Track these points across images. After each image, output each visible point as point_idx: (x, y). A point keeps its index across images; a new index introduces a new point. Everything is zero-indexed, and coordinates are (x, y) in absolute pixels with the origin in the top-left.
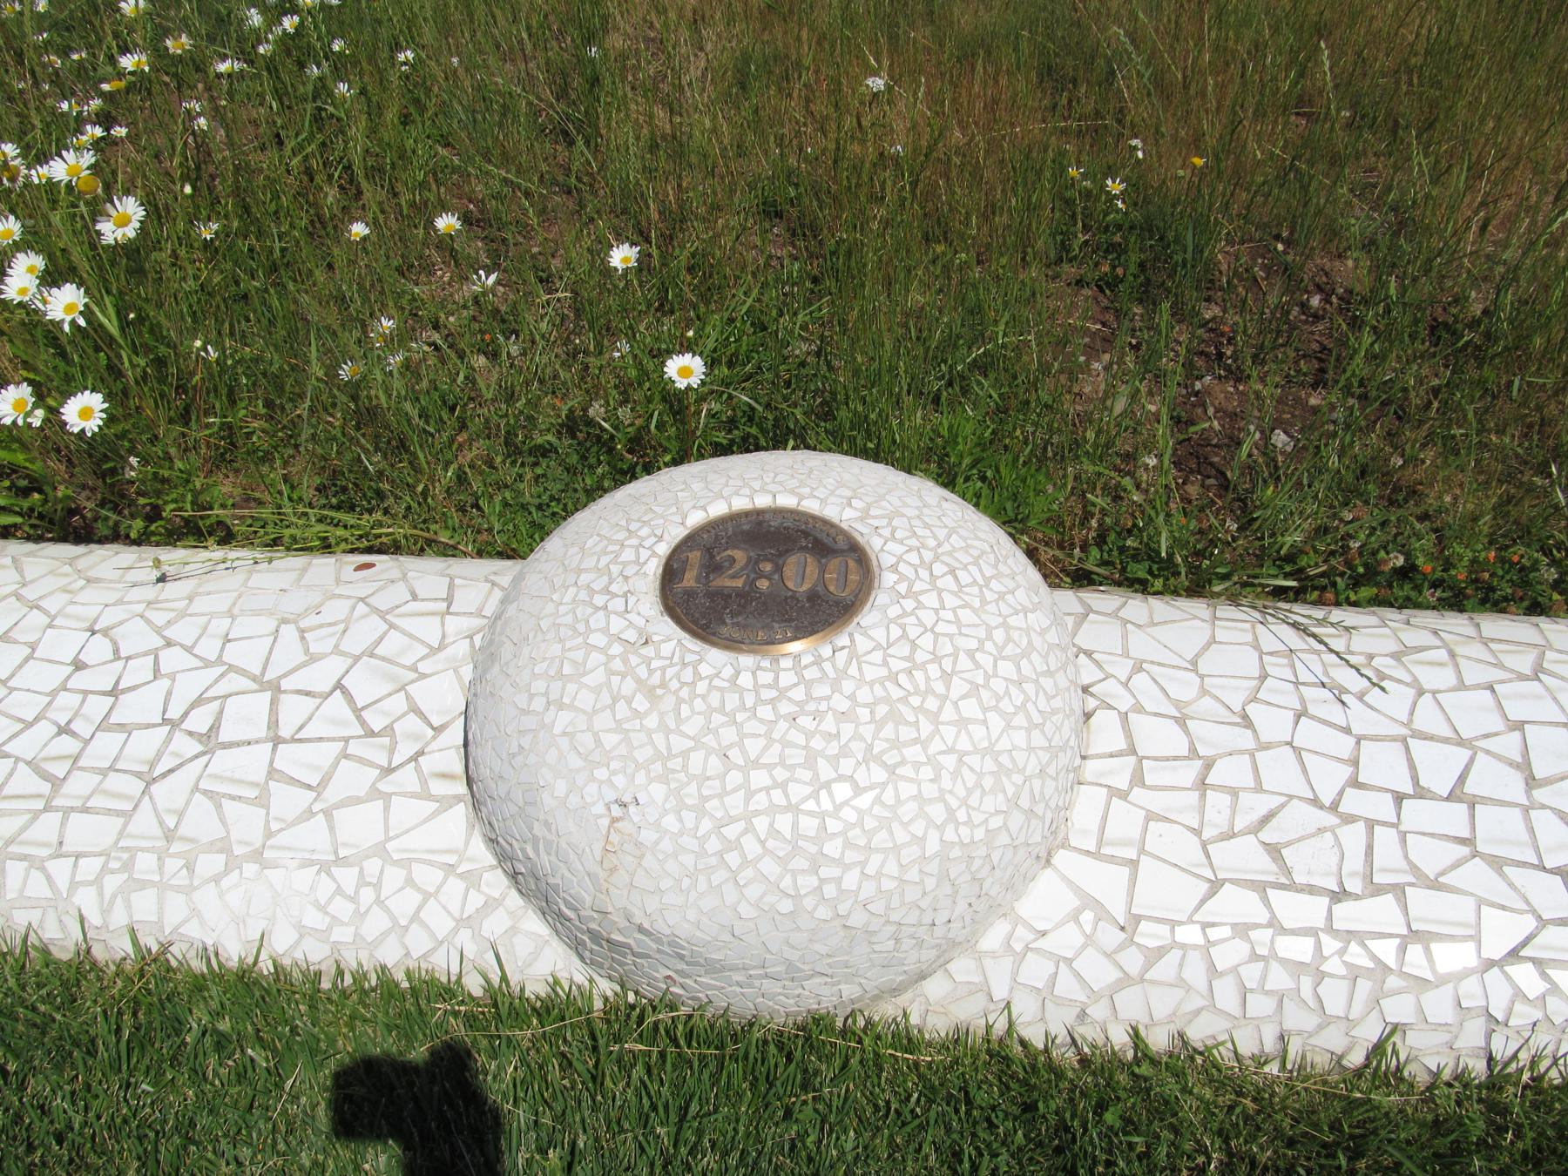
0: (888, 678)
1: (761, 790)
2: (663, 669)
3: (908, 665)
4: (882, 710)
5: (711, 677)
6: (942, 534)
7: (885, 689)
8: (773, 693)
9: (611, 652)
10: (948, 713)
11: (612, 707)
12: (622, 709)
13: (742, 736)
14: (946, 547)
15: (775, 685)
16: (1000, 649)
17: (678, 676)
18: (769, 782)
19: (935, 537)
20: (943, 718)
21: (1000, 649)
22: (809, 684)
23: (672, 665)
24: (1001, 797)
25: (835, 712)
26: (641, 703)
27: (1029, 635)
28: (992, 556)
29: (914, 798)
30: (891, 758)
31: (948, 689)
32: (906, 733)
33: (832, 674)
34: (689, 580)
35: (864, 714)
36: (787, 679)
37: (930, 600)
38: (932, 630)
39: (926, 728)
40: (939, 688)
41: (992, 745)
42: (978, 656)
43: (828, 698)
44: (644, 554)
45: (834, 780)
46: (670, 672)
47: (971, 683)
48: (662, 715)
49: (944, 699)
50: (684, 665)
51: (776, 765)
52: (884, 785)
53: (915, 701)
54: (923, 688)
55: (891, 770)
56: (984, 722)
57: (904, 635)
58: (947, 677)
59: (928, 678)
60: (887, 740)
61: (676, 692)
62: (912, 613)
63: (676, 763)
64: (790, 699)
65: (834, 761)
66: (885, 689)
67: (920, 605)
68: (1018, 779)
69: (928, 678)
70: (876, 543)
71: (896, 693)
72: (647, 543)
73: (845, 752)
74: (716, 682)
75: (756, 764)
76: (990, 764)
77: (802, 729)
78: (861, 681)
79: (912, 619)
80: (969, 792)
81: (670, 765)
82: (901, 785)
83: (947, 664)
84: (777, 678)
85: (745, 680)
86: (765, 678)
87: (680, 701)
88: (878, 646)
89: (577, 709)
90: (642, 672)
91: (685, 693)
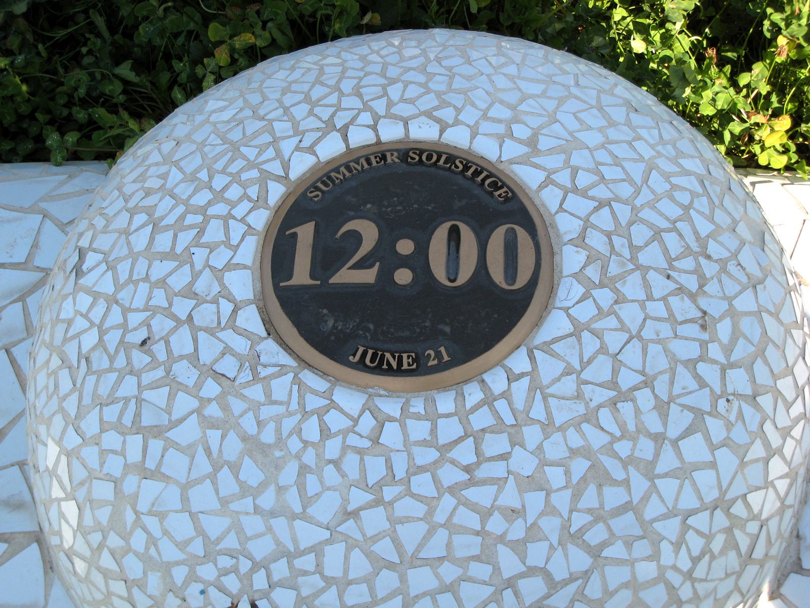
0: (586, 418)
1: (424, 594)
2: (278, 420)
3: (613, 393)
4: (580, 466)
5: (345, 433)
6: (637, 171)
7: (583, 436)
8: (432, 455)
9: (204, 393)
10: (667, 461)
11: (213, 477)
12: (227, 482)
13: (394, 521)
14: (645, 196)
15: (431, 442)
16: (728, 350)
17: (297, 431)
18: (434, 584)
19: (629, 180)
20: (660, 468)
21: (728, 350)
22: (478, 437)
23: (290, 414)
24: (732, 555)
25: (517, 476)
26: (252, 473)
27: (761, 321)
28: (704, 200)
29: (626, 585)
30: (596, 535)
31: (665, 424)
32: (614, 497)
33: (509, 420)
34: (301, 275)
35: (555, 475)
36: (449, 430)
37: (632, 288)
38: (639, 336)
39: (639, 484)
40: (653, 423)
41: (723, 493)
42: (701, 367)
43: (504, 457)
44: (237, 230)
45: (522, 575)
46: (288, 424)
47: (691, 409)
48: (281, 490)
49: (659, 439)
50: (306, 414)
51: (441, 559)
52: (586, 575)
53: (623, 448)
54: (631, 427)
55: (595, 552)
56: (713, 465)
57: (603, 349)
58: (662, 408)
59: (638, 411)
60: (589, 511)
61: (298, 456)
62: (612, 312)
63: (307, 562)
64: (453, 462)
65: (519, 547)
66: (583, 436)
67: (620, 300)
68: (753, 527)
69: (638, 411)
70: (549, 199)
71: (597, 440)
72: (239, 211)
73: (533, 533)
74: (353, 440)
75: (416, 561)
76: (720, 519)
77: (473, 507)
78: (548, 427)
79: (612, 322)
80: (695, 560)
81: (299, 563)
82: (610, 571)
83: (661, 386)
84: (434, 431)
85: (391, 435)
86: (419, 430)
87: (304, 470)
88: (568, 372)
89: (166, 478)
90: (249, 424)
91: (309, 457)
